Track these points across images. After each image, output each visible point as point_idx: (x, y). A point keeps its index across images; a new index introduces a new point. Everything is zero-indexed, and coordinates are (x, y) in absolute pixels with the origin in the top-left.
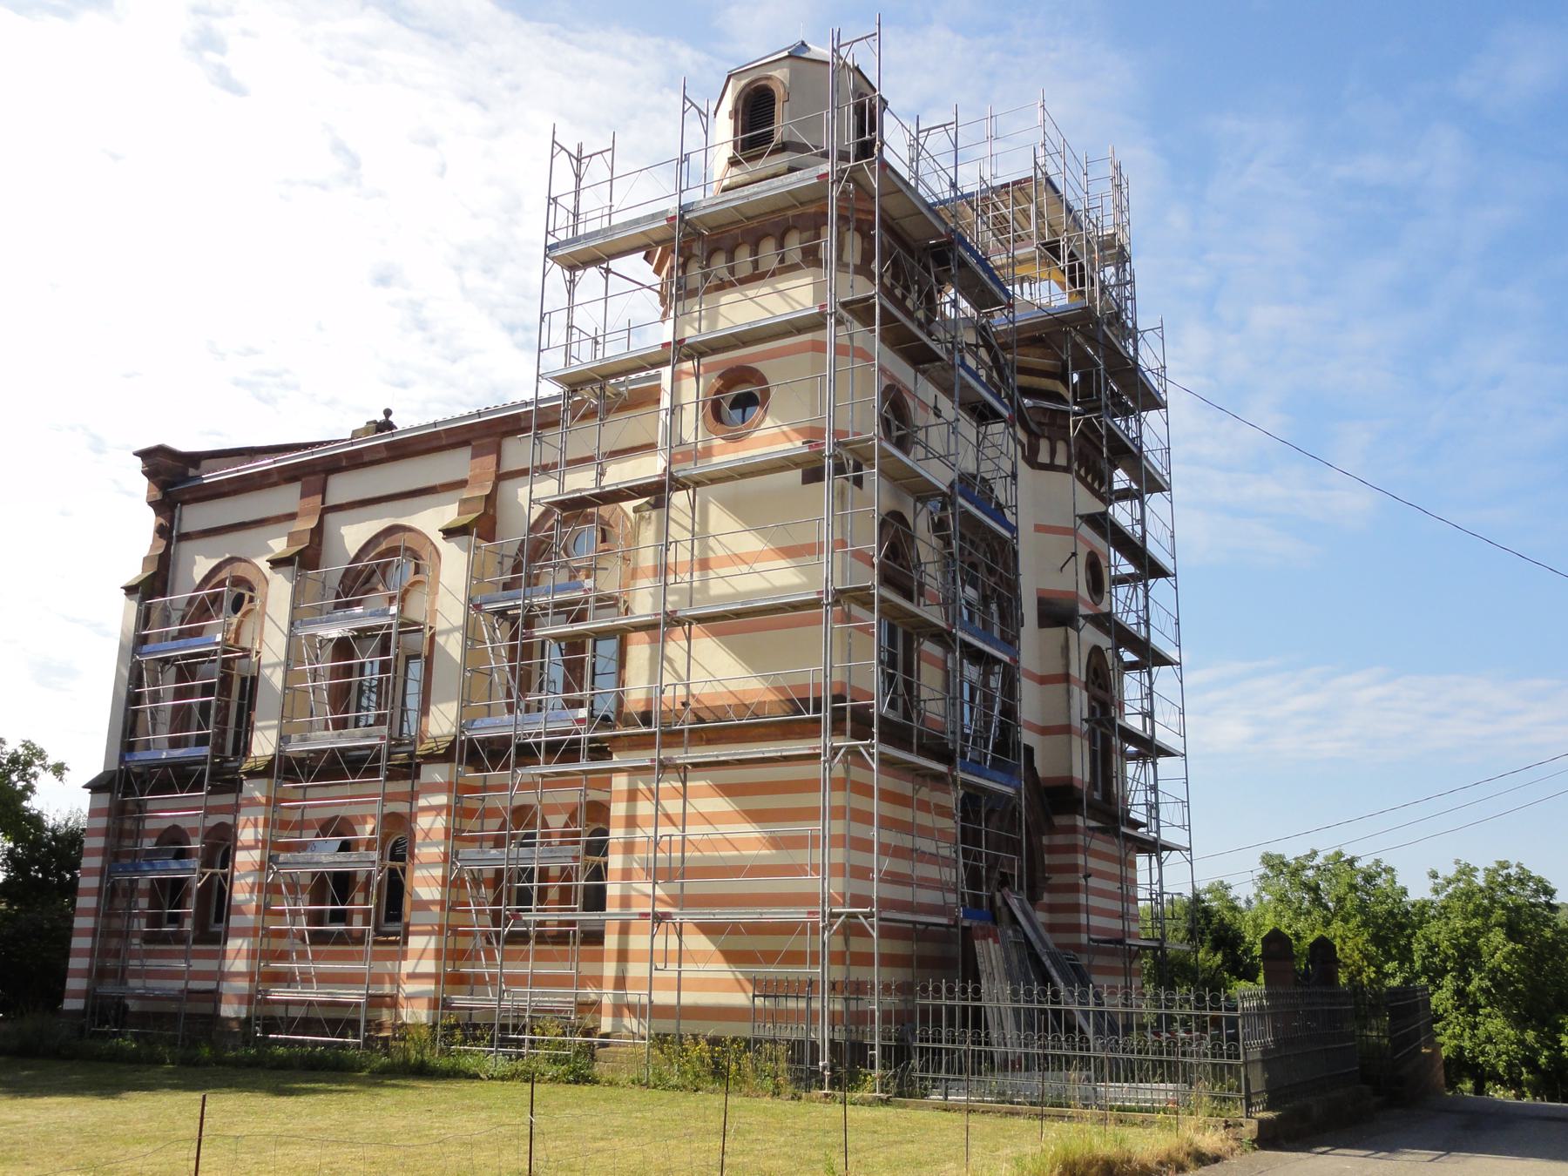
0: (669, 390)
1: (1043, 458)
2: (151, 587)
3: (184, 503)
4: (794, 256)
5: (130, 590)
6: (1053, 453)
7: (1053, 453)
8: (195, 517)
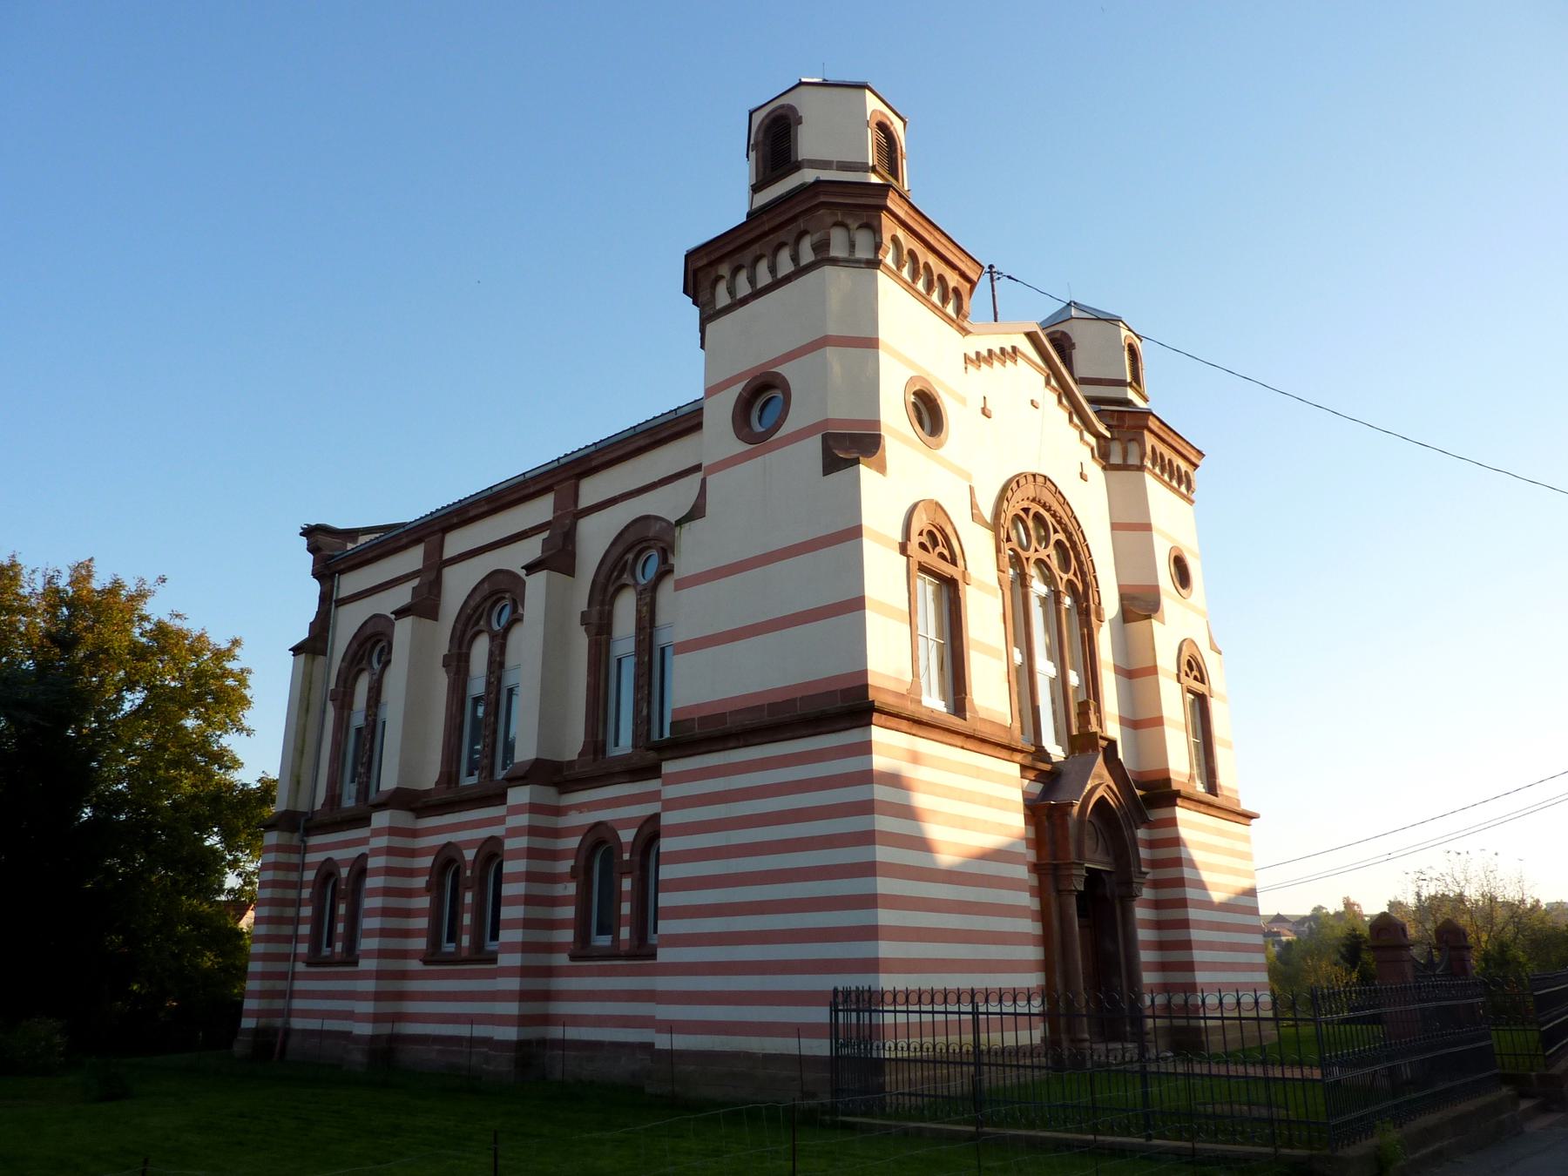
0: (724, 1038)
1: (1116, 459)
2: (311, 648)
3: (341, 572)
4: (807, 256)
5: (297, 650)
6: (1125, 455)
7: (1125, 455)
8: (350, 583)
